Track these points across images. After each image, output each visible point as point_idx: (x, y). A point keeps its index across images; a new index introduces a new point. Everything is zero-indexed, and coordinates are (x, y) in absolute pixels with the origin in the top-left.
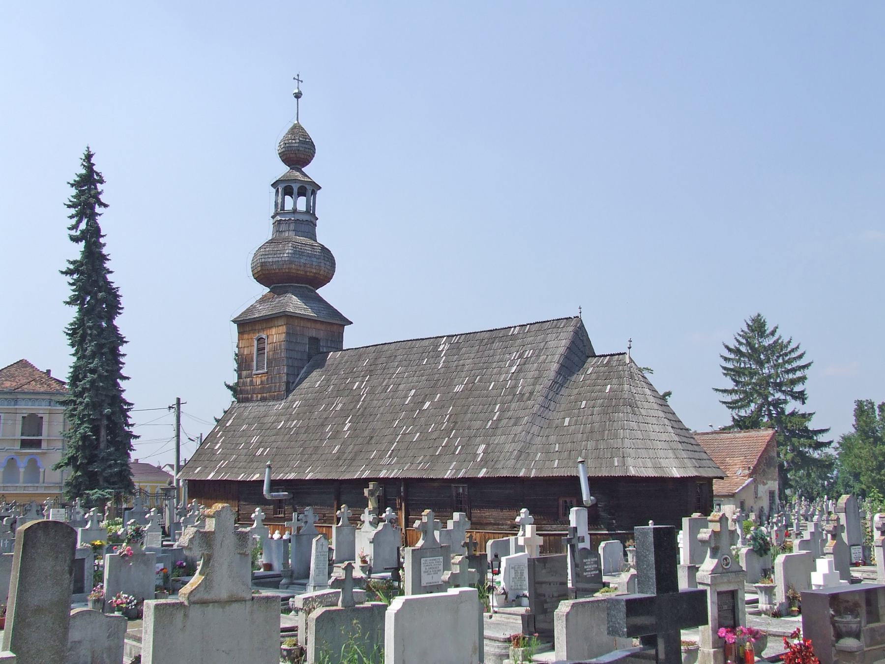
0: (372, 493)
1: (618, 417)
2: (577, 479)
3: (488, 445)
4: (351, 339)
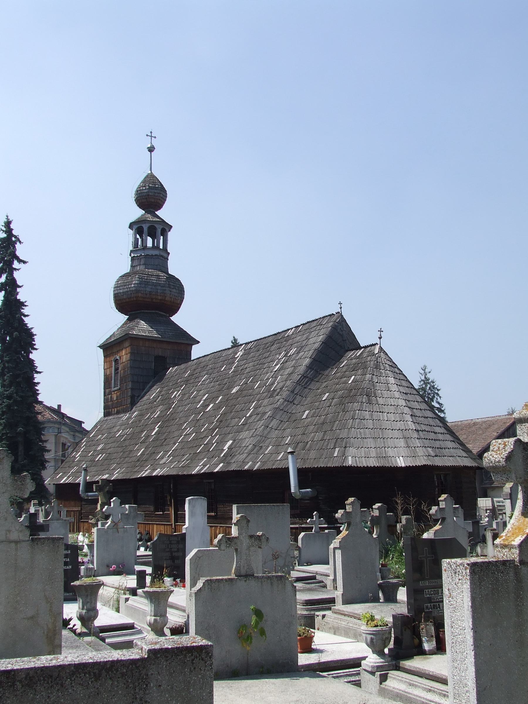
2: (286, 470)
3: (234, 441)
4: (196, 352)
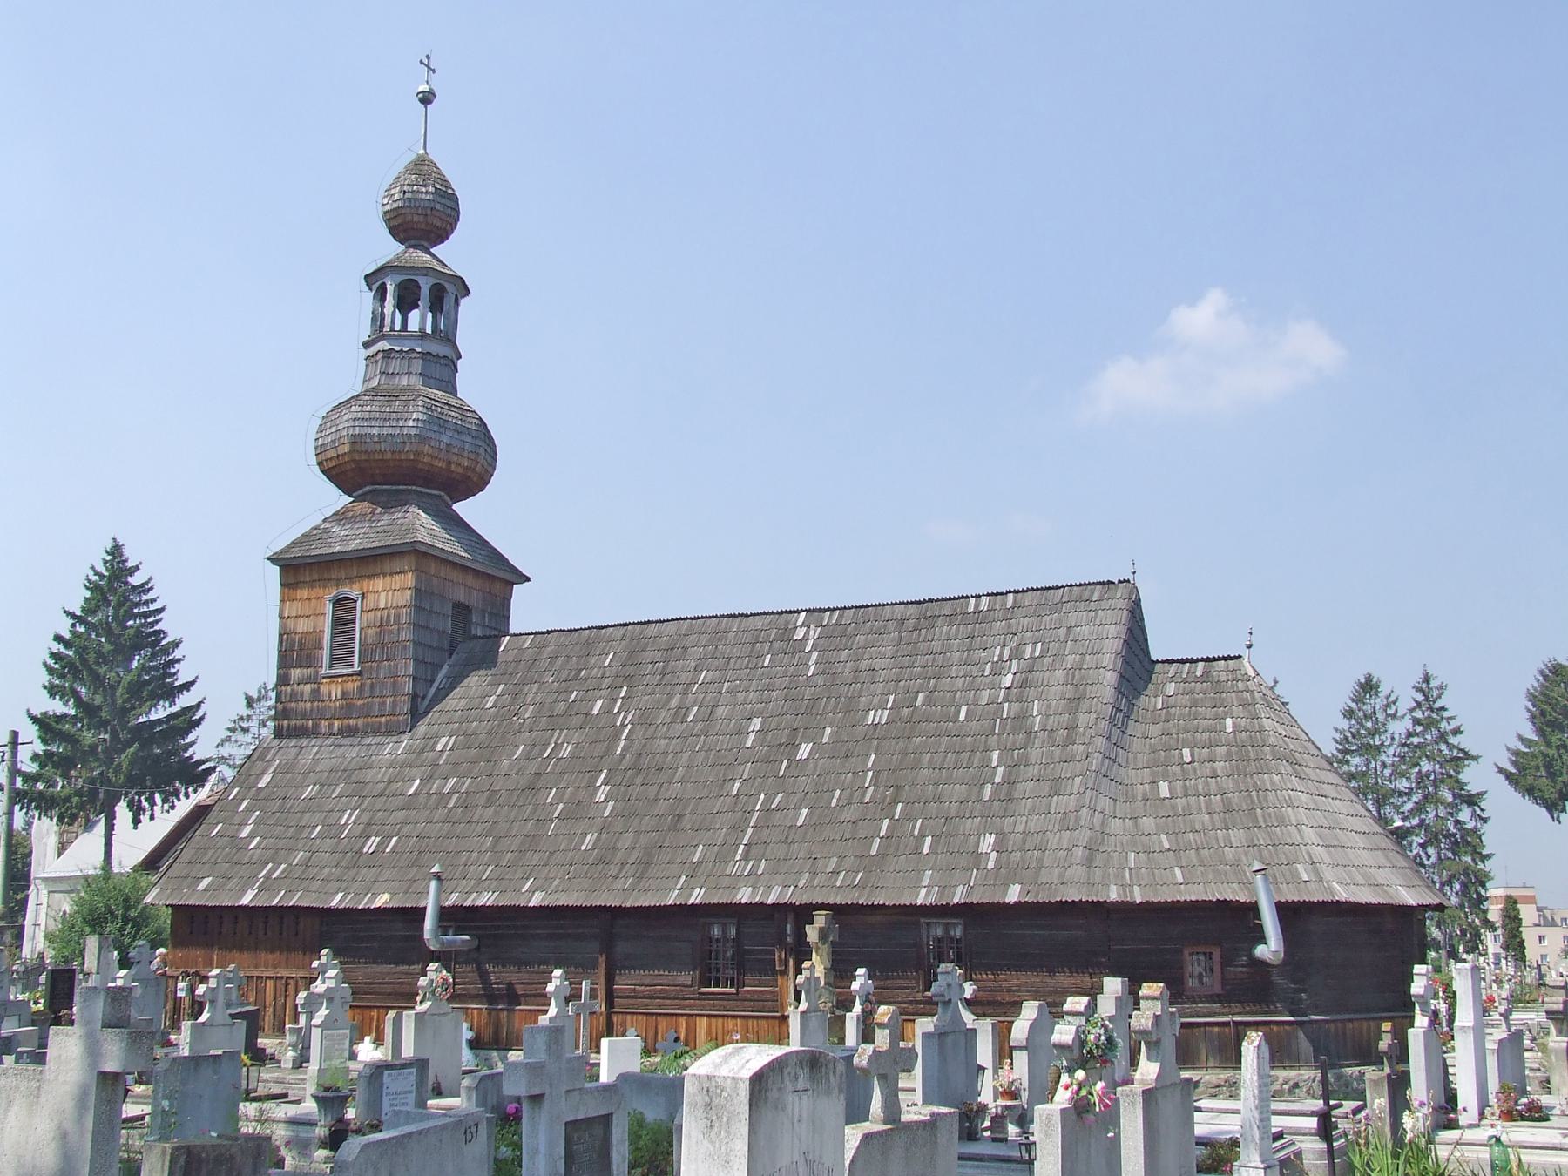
0: (824, 934)
1: (1272, 783)
2: (1253, 909)
3: (1001, 834)
4: (528, 612)
